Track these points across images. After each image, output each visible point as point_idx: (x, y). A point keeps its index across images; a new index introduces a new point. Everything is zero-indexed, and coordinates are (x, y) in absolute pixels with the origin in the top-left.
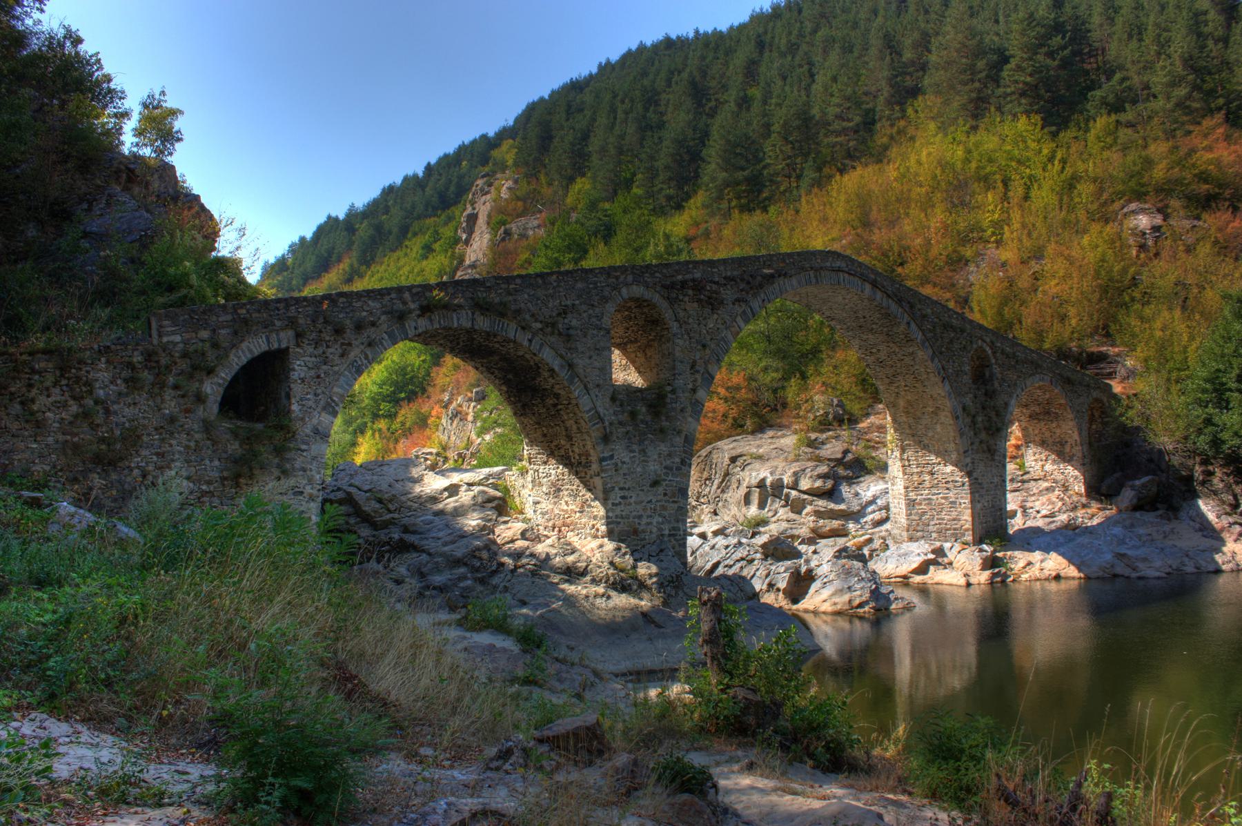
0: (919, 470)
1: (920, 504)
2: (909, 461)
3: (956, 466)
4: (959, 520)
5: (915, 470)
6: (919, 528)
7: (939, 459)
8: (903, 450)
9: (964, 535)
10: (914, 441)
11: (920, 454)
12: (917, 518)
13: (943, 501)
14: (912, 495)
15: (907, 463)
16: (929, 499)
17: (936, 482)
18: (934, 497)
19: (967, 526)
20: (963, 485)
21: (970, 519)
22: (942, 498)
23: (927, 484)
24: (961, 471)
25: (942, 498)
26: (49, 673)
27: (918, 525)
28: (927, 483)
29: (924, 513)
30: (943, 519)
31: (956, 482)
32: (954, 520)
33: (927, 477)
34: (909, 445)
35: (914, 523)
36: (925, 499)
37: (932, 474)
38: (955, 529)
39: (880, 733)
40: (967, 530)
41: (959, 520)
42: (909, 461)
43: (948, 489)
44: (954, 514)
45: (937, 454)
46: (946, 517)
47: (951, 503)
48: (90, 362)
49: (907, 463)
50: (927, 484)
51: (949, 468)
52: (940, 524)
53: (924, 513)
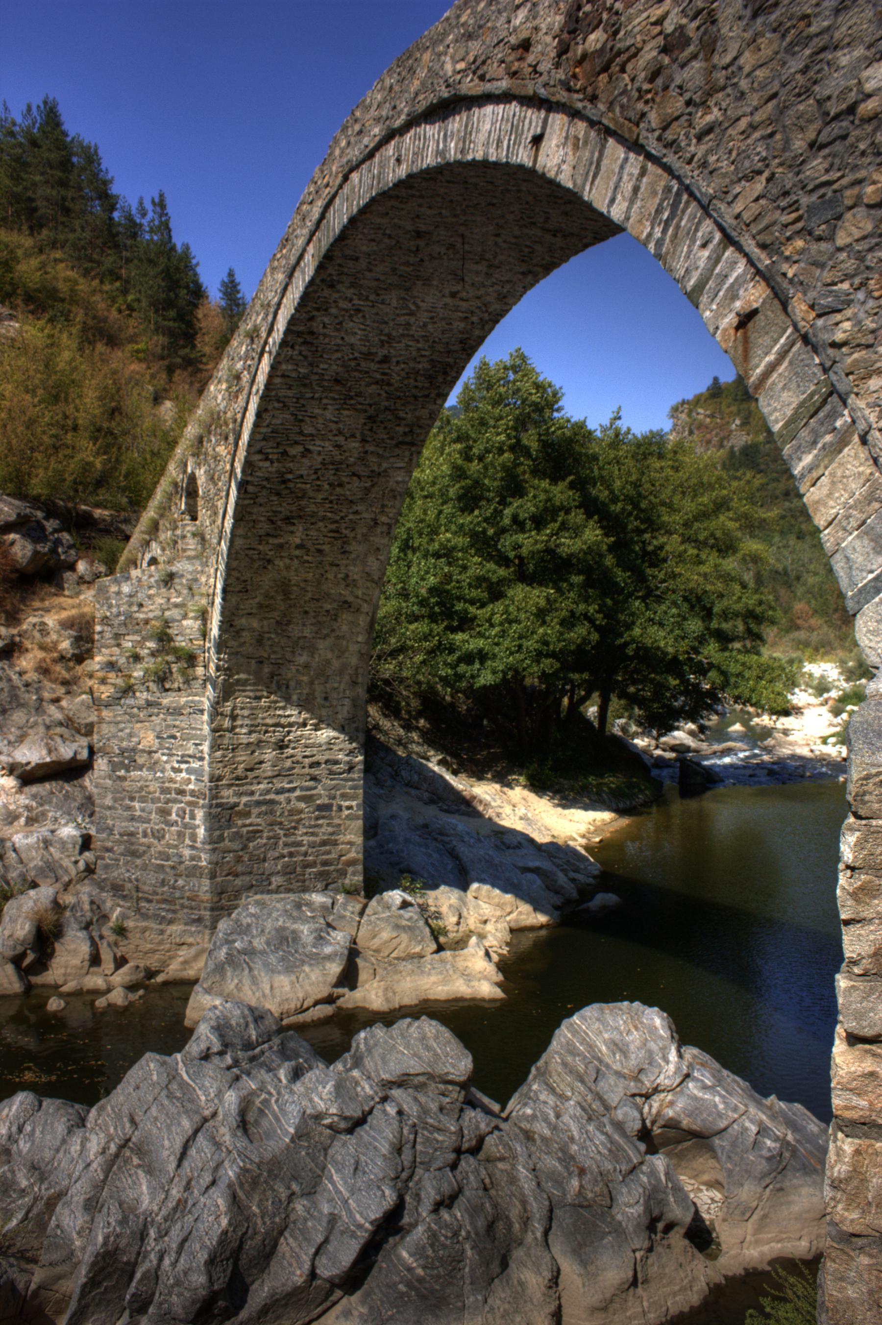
0: (254, 738)
1: (248, 814)
2: (234, 718)
3: (342, 729)
4: (335, 843)
5: (244, 740)
6: (240, 868)
7: (304, 715)
8: (226, 692)
9: (343, 873)
10: (257, 674)
11: (263, 702)
12: (236, 845)
13: (303, 805)
14: (228, 795)
15: (227, 723)
16: (272, 802)
17: (288, 763)
18: (281, 798)
19: (353, 855)
20: (351, 769)
21: (359, 840)
22: (299, 799)
23: (267, 769)
24: (351, 741)
25: (299, 799)
26: (359, 1089)
27: (239, 860)
28: (266, 766)
29: (255, 834)
30: (299, 844)
31: (336, 762)
32: (324, 843)
33: (269, 754)
34: (245, 683)
35: (229, 857)
36: (258, 803)
37: (281, 746)
38: (325, 863)
39: (241, 1168)
40: (352, 863)
41: (335, 843)
42: (234, 718)
43: (314, 778)
44: (324, 831)
45: (303, 705)
46: (306, 839)
47: (320, 808)
48: (99, 1122)
49: (227, 723)
50: (267, 769)
51: (326, 734)
52: (291, 855)
53: (255, 834)
